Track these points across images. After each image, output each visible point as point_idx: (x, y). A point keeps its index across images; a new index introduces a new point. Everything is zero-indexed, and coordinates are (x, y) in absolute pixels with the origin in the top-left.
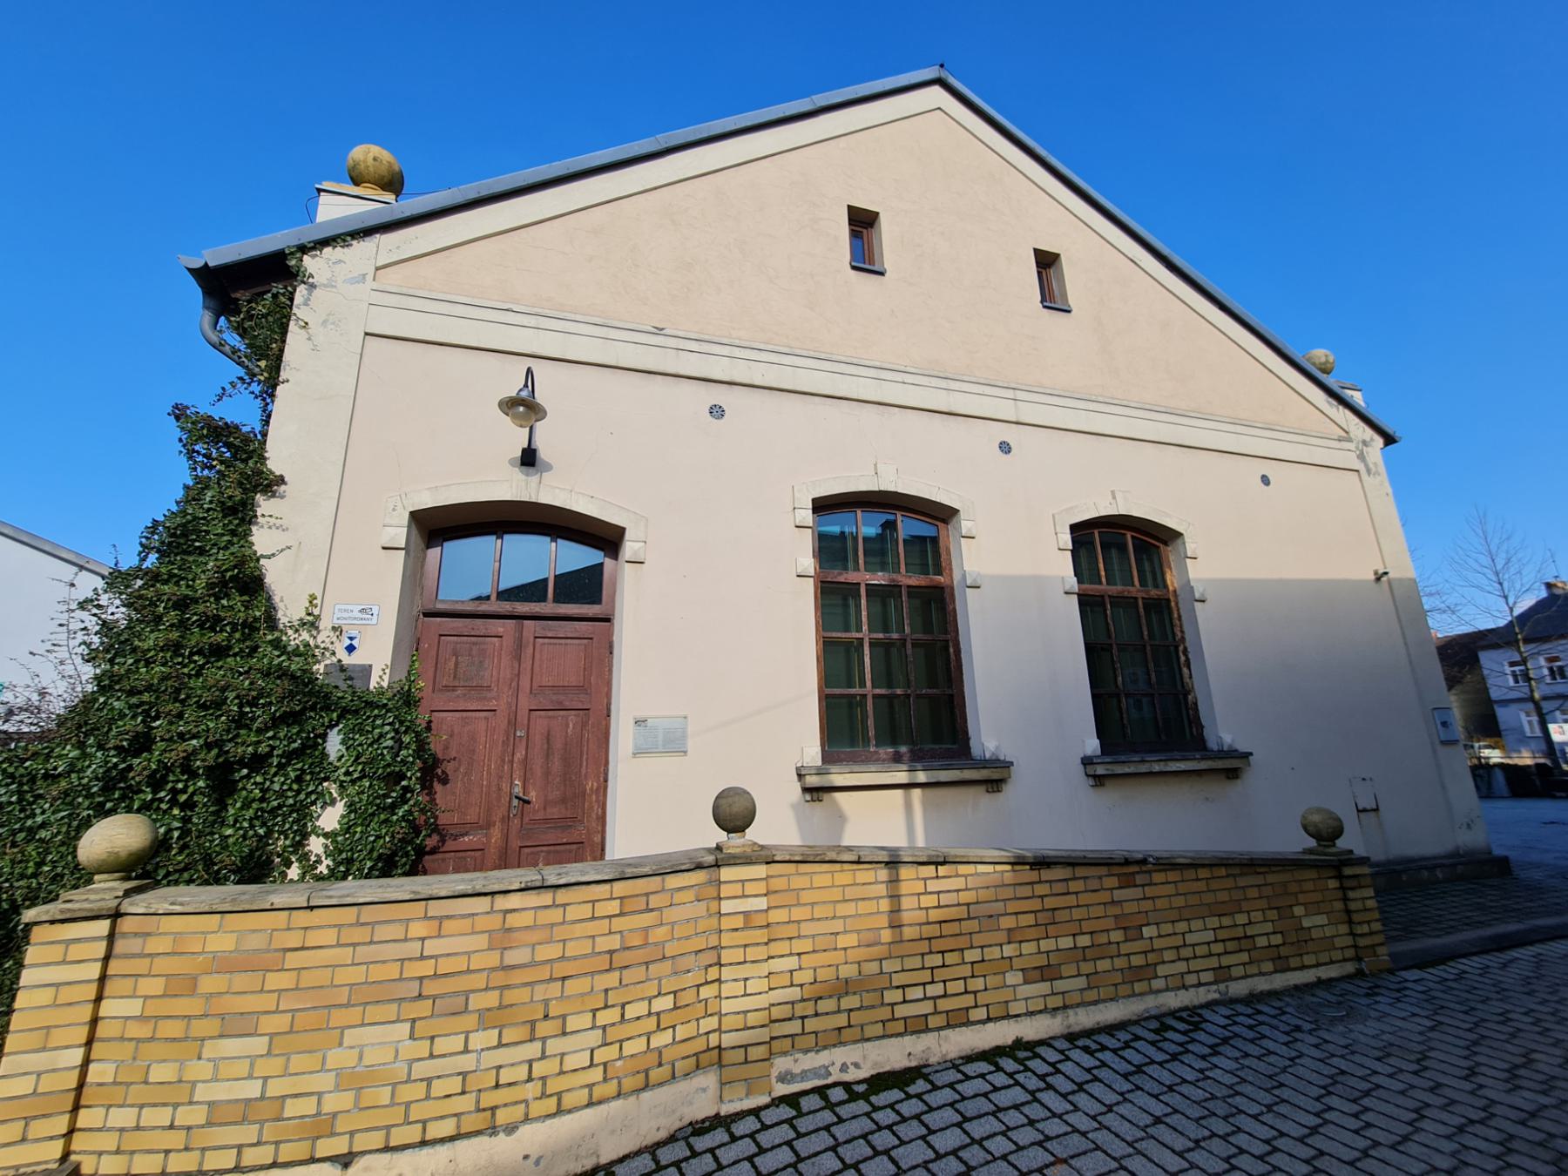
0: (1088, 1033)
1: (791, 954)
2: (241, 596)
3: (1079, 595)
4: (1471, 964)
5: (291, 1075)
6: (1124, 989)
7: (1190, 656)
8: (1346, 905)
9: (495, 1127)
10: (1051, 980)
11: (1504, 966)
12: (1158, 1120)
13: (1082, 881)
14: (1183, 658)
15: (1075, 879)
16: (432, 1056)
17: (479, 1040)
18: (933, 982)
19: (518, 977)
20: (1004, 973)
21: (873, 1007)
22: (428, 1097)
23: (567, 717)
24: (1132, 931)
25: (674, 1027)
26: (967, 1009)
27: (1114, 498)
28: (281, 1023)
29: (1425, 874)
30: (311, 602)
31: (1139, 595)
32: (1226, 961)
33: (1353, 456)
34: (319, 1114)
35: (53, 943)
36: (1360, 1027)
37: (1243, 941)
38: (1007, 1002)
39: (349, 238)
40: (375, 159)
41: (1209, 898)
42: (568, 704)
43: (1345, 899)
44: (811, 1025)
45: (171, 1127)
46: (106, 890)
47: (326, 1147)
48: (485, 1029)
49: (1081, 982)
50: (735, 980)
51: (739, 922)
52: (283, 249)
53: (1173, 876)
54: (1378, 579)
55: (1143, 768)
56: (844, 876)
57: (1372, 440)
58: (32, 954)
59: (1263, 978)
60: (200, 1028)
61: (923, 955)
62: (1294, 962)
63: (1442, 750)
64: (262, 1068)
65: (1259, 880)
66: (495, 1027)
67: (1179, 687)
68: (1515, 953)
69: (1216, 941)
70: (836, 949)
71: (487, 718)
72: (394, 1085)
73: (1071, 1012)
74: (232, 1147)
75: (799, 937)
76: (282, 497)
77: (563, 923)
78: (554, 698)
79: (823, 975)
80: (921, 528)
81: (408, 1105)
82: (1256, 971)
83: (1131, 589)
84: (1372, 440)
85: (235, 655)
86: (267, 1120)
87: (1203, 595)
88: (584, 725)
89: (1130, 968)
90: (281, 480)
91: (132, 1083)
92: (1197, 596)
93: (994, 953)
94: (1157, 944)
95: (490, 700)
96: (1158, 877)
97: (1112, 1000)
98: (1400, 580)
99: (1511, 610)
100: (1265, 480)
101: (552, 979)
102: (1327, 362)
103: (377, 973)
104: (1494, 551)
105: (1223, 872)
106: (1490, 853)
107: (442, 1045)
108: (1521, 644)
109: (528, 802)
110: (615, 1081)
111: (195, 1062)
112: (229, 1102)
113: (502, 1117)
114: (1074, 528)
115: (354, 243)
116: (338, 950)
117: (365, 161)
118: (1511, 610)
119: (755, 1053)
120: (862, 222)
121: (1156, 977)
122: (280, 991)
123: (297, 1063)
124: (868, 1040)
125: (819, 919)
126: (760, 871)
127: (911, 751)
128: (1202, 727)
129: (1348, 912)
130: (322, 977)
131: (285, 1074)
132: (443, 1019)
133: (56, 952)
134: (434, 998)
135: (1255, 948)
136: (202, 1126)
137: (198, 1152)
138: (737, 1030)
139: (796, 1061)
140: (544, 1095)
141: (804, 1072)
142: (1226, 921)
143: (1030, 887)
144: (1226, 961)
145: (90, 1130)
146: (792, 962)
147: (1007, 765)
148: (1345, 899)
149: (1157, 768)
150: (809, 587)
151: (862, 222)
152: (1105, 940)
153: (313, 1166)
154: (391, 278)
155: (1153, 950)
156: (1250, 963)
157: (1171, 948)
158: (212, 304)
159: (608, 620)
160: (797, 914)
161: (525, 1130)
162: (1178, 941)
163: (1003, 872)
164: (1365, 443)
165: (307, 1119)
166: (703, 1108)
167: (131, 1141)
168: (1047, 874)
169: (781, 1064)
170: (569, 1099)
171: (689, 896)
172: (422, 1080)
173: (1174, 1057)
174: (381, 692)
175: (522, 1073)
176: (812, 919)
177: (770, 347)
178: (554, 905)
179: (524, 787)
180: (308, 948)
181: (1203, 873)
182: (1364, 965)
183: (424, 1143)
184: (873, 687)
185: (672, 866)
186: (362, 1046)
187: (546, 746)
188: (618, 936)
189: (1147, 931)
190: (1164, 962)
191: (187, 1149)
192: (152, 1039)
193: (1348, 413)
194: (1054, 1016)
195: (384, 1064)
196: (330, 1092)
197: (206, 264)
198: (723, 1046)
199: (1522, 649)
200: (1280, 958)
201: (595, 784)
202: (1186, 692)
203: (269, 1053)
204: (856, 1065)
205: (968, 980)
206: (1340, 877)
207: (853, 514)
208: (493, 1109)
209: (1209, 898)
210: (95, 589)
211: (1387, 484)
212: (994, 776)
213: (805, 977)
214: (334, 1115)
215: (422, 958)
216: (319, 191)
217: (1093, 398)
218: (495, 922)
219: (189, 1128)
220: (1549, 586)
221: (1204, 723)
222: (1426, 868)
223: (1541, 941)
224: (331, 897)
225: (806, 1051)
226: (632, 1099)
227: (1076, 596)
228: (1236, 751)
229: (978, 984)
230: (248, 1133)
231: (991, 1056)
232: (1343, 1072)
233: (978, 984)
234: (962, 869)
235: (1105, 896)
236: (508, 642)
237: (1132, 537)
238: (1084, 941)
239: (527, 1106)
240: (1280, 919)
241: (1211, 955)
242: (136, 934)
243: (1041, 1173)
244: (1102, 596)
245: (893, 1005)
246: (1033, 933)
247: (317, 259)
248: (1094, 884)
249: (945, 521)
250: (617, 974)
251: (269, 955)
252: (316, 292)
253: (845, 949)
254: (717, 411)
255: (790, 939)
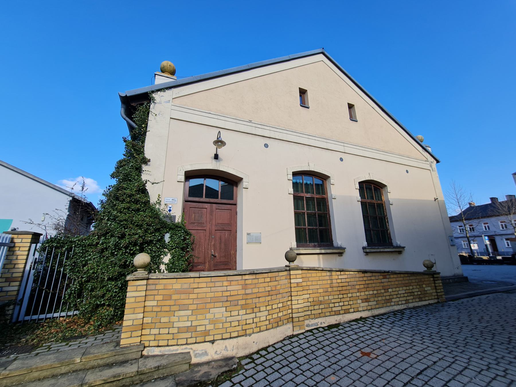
0: (378, 316)
1: (307, 294)
2: (142, 194)
3: (361, 202)
4: (465, 300)
5: (198, 320)
6: (385, 305)
7: (388, 220)
8: (435, 285)
9: (246, 334)
10: (368, 302)
11: (472, 300)
12: (402, 331)
13: (374, 277)
14: (386, 220)
15: (372, 276)
16: (231, 316)
17: (242, 312)
18: (341, 302)
19: (249, 297)
20: (357, 300)
21: (327, 308)
22: (231, 326)
23: (225, 232)
24: (386, 290)
25: (283, 311)
26: (349, 309)
27: (369, 175)
28: (194, 307)
29: (448, 281)
30: (159, 197)
31: (375, 202)
32: (408, 298)
33: (429, 166)
34: (205, 330)
35: (133, 286)
36: (442, 313)
37: (412, 293)
38: (358, 307)
39: (165, 89)
40: (170, 66)
41: (404, 282)
42: (225, 229)
43: (435, 283)
44: (313, 312)
45: (169, 333)
46: (141, 273)
47: (208, 338)
48: (242, 310)
49: (375, 303)
50: (295, 300)
51: (295, 285)
52: (147, 92)
53: (395, 276)
54: (435, 200)
55: (378, 250)
56: (319, 274)
57: (433, 161)
58: (129, 289)
59: (416, 303)
60: (173, 308)
61: (338, 295)
62: (423, 299)
63: (452, 248)
64: (191, 318)
65: (415, 278)
66: (245, 309)
67: (385, 228)
68: (474, 298)
69: (405, 293)
70: (318, 293)
71: (203, 232)
72: (223, 323)
73: (373, 310)
74: (185, 338)
75: (309, 289)
76: (149, 165)
77: (258, 283)
78: (222, 227)
79: (315, 299)
80: (319, 182)
81: (226, 328)
82: (415, 301)
83: (373, 201)
84: (433, 161)
85: (141, 211)
86: (193, 332)
87: (392, 203)
88: (230, 235)
89: (386, 299)
90: (149, 161)
91: (156, 323)
92: (391, 203)
93: (354, 295)
94: (392, 293)
95: (204, 227)
96: (392, 276)
97: (382, 307)
98: (441, 200)
99: (461, 210)
100: (407, 172)
101: (257, 298)
102: (422, 139)
103: (217, 295)
104: (457, 193)
105: (407, 275)
106: (463, 275)
107: (233, 313)
108: (464, 220)
109: (215, 257)
110: (271, 324)
111: (173, 317)
112: (183, 327)
113: (248, 332)
114: (360, 183)
115: (166, 91)
116: (207, 289)
117: (167, 66)
118: (461, 210)
119: (301, 319)
120: (303, 92)
121: (392, 302)
122: (193, 299)
123: (199, 317)
124: (327, 316)
125: (314, 285)
126: (300, 272)
127: (318, 244)
128: (392, 240)
129: (435, 286)
130: (204, 295)
131: (197, 320)
132: (233, 307)
133: (134, 288)
134: (230, 301)
135: (415, 295)
136: (177, 333)
137: (176, 340)
138: (296, 313)
139: (310, 321)
140: (256, 327)
141: (312, 324)
142: (408, 288)
143: (362, 278)
144: (408, 298)
145: (146, 335)
146: (308, 296)
147: (344, 249)
148: (435, 283)
149: (382, 250)
150: (292, 196)
151: (303, 92)
152: (380, 292)
153: (205, 343)
154: (177, 101)
155: (391, 295)
156: (413, 299)
157: (395, 295)
158: (124, 106)
159: (236, 205)
160: (309, 283)
161: (253, 335)
162: (396, 293)
163: (356, 274)
164: (432, 162)
165: (203, 332)
166: (290, 333)
167: (158, 337)
168: (366, 275)
169: (307, 322)
170: (262, 328)
171: (284, 278)
172: (229, 322)
173: (400, 320)
174: (179, 223)
175: (251, 321)
176: (312, 285)
177: (280, 128)
178: (256, 279)
179: (214, 253)
180: (199, 288)
181: (402, 275)
182: (439, 300)
183: (231, 338)
184: (308, 226)
185: (281, 270)
186: (214, 313)
187: (220, 241)
188: (270, 287)
189: (390, 290)
190: (394, 298)
191: (173, 339)
192: (161, 311)
193: (428, 154)
194: (369, 311)
195: (220, 318)
196: (208, 325)
197: (126, 95)
198: (293, 317)
199: (464, 222)
200: (420, 298)
201: (234, 252)
202: (387, 230)
203: (192, 315)
204: (324, 323)
205: (349, 302)
206: (433, 277)
207: (301, 177)
208: (246, 330)
209: (404, 282)
210: (105, 191)
211: (437, 174)
212: (340, 252)
213: (311, 300)
214: (209, 330)
215: (227, 291)
216: (155, 74)
217: (364, 147)
218: (243, 282)
219: (173, 334)
220: (470, 204)
221: (392, 239)
222: (448, 279)
223: (480, 295)
224: (205, 275)
225: (312, 319)
226: (275, 329)
227: (360, 202)
228: (401, 246)
229: (351, 303)
230: (189, 335)
231: (356, 320)
232: (441, 322)
233: (351, 303)
234: (347, 273)
235: (379, 281)
236: (209, 210)
237: (374, 186)
238: (375, 292)
239: (253, 330)
240: (420, 288)
241: (404, 297)
242: (153, 284)
243: (316, 386)
244: (366, 202)
245: (332, 307)
246: (364, 290)
247: (156, 95)
248: (377, 278)
249: (325, 180)
250: (270, 297)
251: (190, 289)
252: (156, 105)
253: (320, 293)
254: (266, 146)
255: (307, 290)
